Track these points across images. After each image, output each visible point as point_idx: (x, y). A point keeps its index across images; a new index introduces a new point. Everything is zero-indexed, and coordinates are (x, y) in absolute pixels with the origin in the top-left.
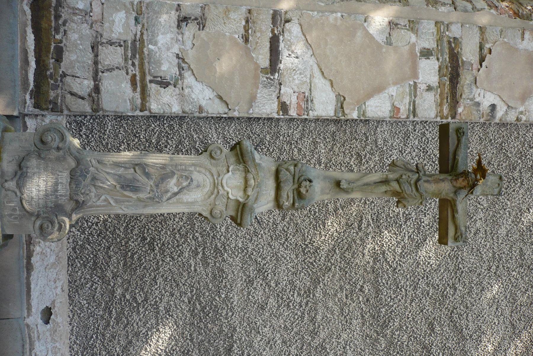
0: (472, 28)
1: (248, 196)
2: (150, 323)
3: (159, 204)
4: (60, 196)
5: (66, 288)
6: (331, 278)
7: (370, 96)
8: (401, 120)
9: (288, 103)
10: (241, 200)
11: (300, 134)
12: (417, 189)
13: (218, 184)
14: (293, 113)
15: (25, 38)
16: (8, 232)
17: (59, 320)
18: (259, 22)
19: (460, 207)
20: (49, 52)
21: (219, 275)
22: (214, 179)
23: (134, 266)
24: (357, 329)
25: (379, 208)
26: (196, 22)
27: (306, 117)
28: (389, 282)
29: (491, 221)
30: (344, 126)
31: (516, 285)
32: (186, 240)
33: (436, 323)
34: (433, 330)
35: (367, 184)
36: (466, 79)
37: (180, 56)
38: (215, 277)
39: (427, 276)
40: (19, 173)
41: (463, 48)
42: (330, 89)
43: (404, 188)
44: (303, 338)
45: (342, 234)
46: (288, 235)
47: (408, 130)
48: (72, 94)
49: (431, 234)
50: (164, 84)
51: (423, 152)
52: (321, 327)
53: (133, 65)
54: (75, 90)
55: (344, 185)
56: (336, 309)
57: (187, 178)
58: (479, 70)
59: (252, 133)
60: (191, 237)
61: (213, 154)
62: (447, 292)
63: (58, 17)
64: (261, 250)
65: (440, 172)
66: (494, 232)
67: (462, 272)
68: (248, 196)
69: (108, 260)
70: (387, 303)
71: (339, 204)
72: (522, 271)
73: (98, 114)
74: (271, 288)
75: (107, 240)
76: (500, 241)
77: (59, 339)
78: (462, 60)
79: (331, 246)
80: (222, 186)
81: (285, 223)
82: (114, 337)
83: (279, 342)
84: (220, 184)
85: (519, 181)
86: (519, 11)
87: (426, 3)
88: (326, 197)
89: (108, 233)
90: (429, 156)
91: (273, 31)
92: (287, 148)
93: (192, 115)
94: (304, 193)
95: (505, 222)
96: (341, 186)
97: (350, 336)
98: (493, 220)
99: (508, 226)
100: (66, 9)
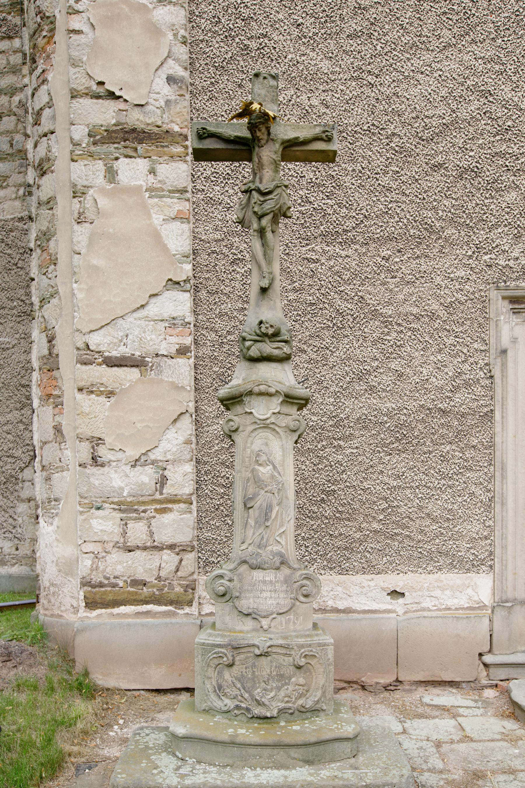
0: (75, 110)
1: (277, 391)
2: (410, 495)
3: (285, 484)
4: (276, 578)
5: (370, 577)
6: (372, 296)
7: (165, 248)
8: (192, 209)
9: (177, 347)
10: (281, 400)
11: (211, 332)
12: (270, 193)
13: (264, 424)
14: (188, 341)
15: (124, 614)
16: (311, 625)
17: (401, 584)
18: (91, 379)
19: (291, 135)
20: (136, 593)
21: (363, 423)
22: (259, 428)
23: (350, 511)
24: (431, 264)
25: (294, 237)
26: (96, 448)
27: (192, 325)
28: (380, 224)
29: (312, 82)
30: (201, 280)
31: (394, 43)
32: (325, 457)
33: (433, 162)
34: (440, 165)
35: (265, 254)
36: (138, 120)
37: (133, 463)
38: (365, 428)
39: (376, 173)
40: (254, 616)
41: (101, 123)
42: (159, 297)
43: (268, 209)
44: (437, 329)
45: (322, 282)
46: (322, 346)
47: (203, 200)
48: (177, 570)
49: (325, 169)
50: (163, 481)
51: (229, 179)
52: (426, 308)
53: (144, 511)
54: (173, 568)
55: (265, 283)
56: (406, 290)
57: (258, 455)
58: (126, 101)
59: (211, 387)
60: (322, 452)
61: (233, 429)
62: (397, 146)
63: (101, 585)
64: (337, 377)
65: (250, 160)
66: (326, 79)
67: (373, 125)
68: (277, 391)
69: (343, 536)
70: (404, 227)
71: (289, 287)
72: (376, 34)
73: (196, 546)
74: (380, 366)
75: (323, 538)
76: (338, 69)
77: (420, 584)
78: (115, 125)
79: (335, 296)
80: (267, 419)
81: (309, 350)
82: (422, 531)
83: (439, 358)
84: (264, 422)
85: (262, 40)
86: (44, 37)
87: (50, 174)
88: (279, 305)
89: (316, 536)
90: (233, 171)
91: (100, 364)
92: (227, 347)
93: (195, 451)
94: (273, 330)
95: (313, 63)
96: (267, 287)
97: (439, 273)
98: (311, 80)
99: (319, 58)
100: (93, 577)
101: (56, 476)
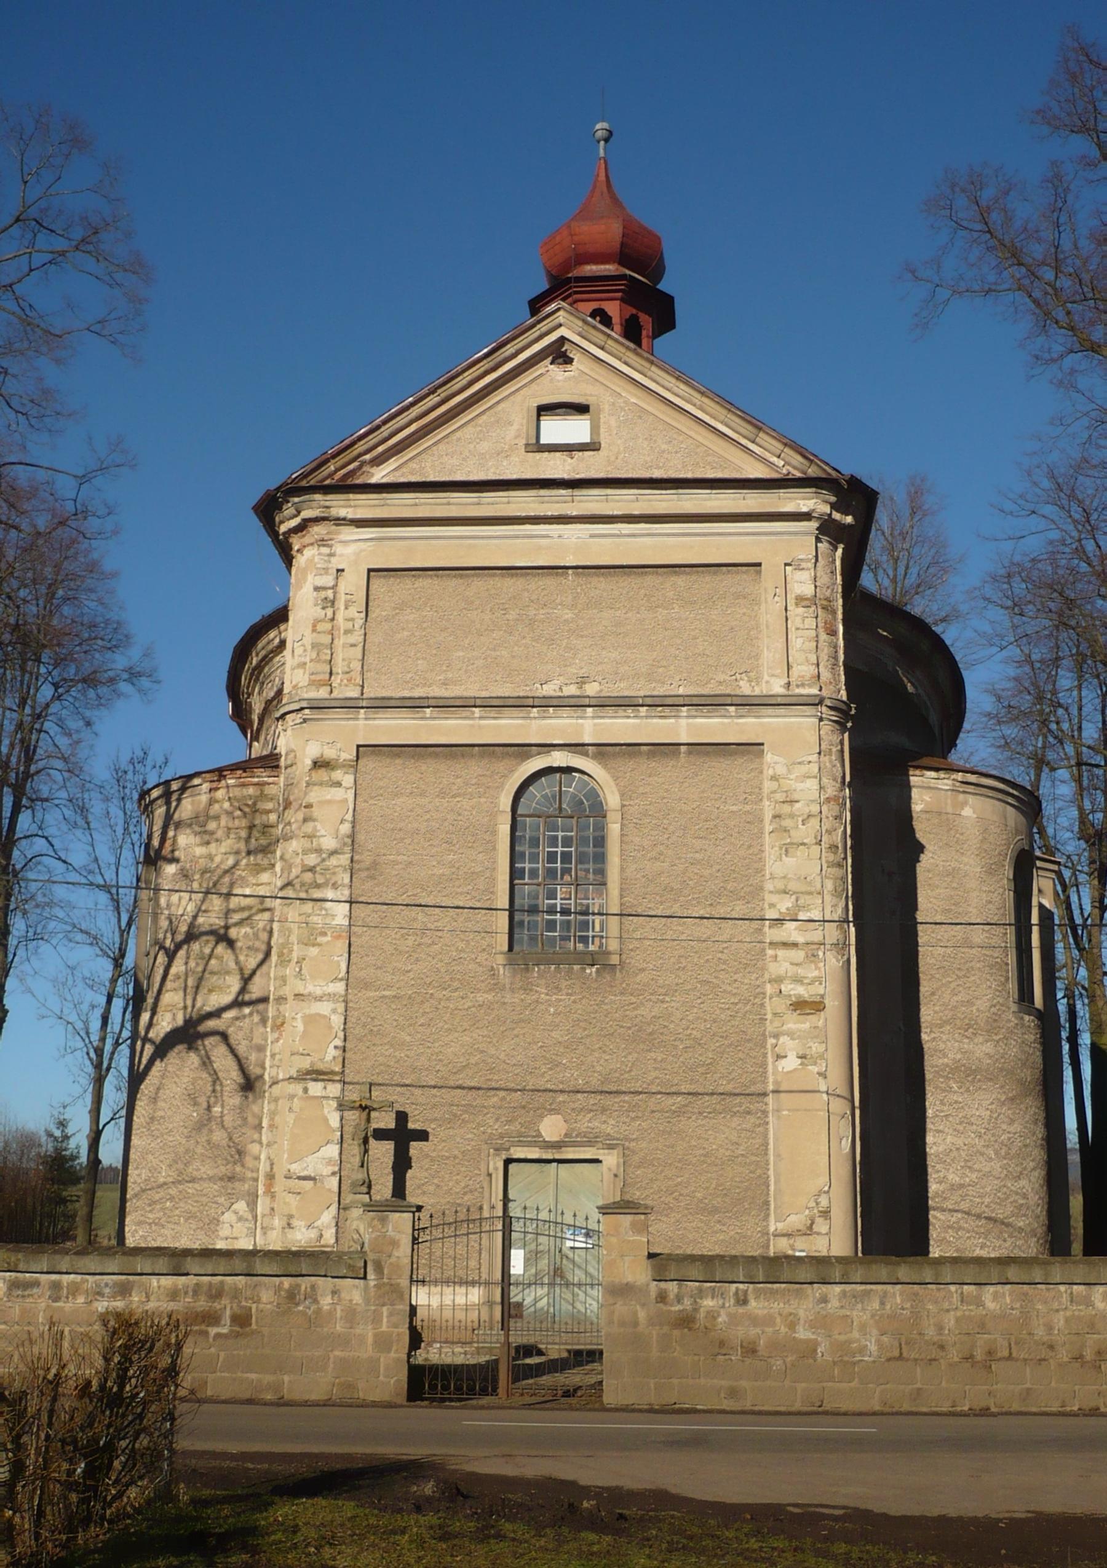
50: (321, 1236)
56: (443, 1144)
101: (269, 1233)
